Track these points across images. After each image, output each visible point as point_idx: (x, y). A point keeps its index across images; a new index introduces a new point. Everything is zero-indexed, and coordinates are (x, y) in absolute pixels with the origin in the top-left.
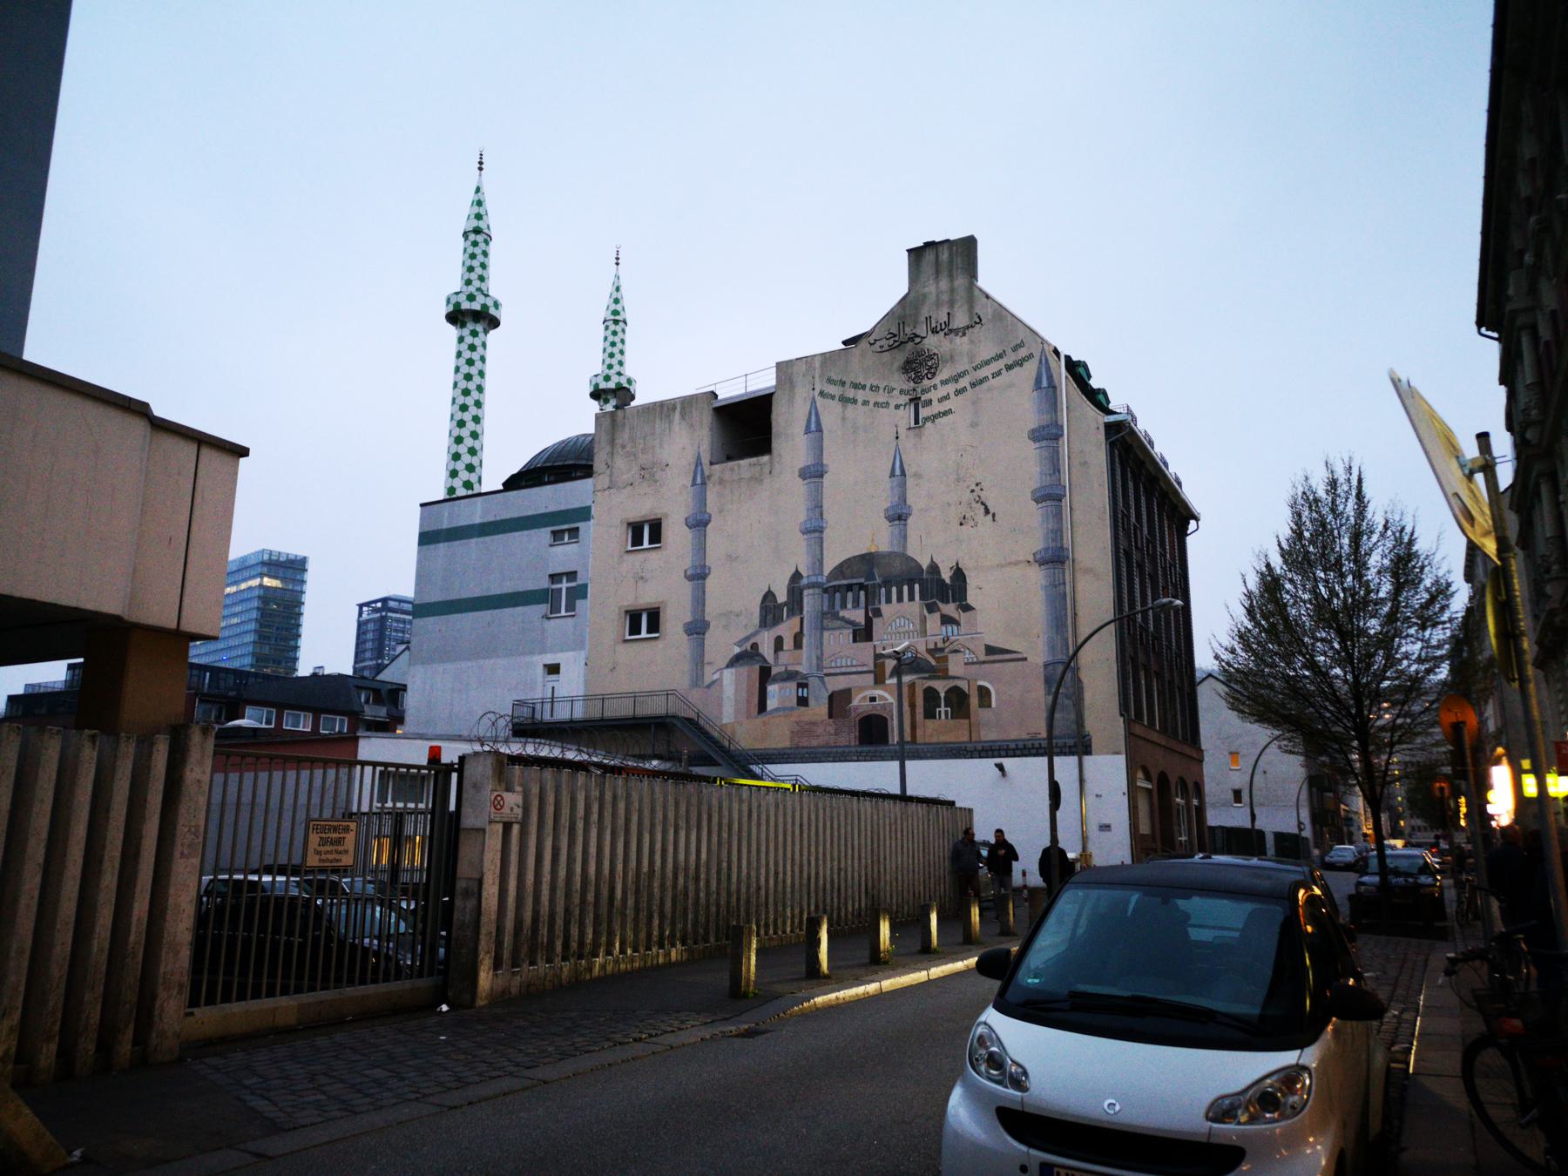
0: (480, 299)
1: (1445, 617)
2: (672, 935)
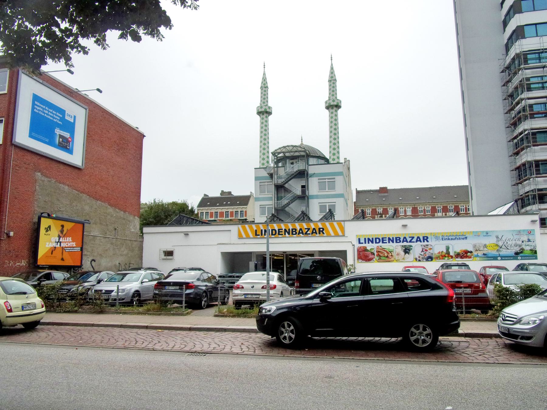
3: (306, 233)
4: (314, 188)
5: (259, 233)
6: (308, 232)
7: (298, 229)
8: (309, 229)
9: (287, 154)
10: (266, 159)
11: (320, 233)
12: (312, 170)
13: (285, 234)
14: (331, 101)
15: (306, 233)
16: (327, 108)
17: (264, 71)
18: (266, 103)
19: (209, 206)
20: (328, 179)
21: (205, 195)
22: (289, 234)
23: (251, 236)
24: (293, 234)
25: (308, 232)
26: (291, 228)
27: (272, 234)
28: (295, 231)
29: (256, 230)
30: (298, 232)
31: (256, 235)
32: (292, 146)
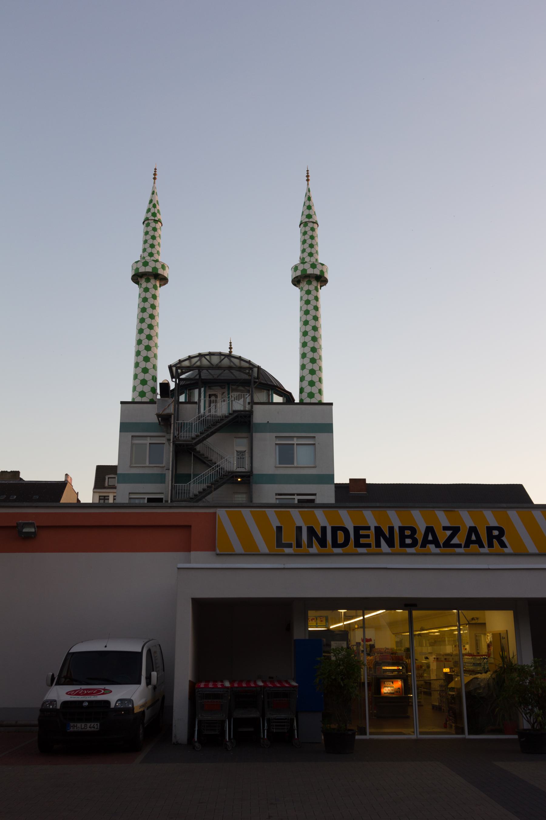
0: (152, 264)
1: (422, 683)
2: (187, 430)
3: (447, 544)
5: (289, 537)
6: (455, 541)
7: (421, 528)
8: (455, 530)
9: (205, 375)
11: (491, 545)
12: (261, 415)
13: (378, 545)
14: (307, 266)
15: (447, 544)
16: (296, 282)
20: (298, 437)
22: (391, 544)
23: (263, 548)
24: (403, 545)
25: (455, 541)
26: (397, 524)
27: (335, 544)
28: (411, 537)
29: (279, 529)
30: (419, 536)
31: (280, 544)
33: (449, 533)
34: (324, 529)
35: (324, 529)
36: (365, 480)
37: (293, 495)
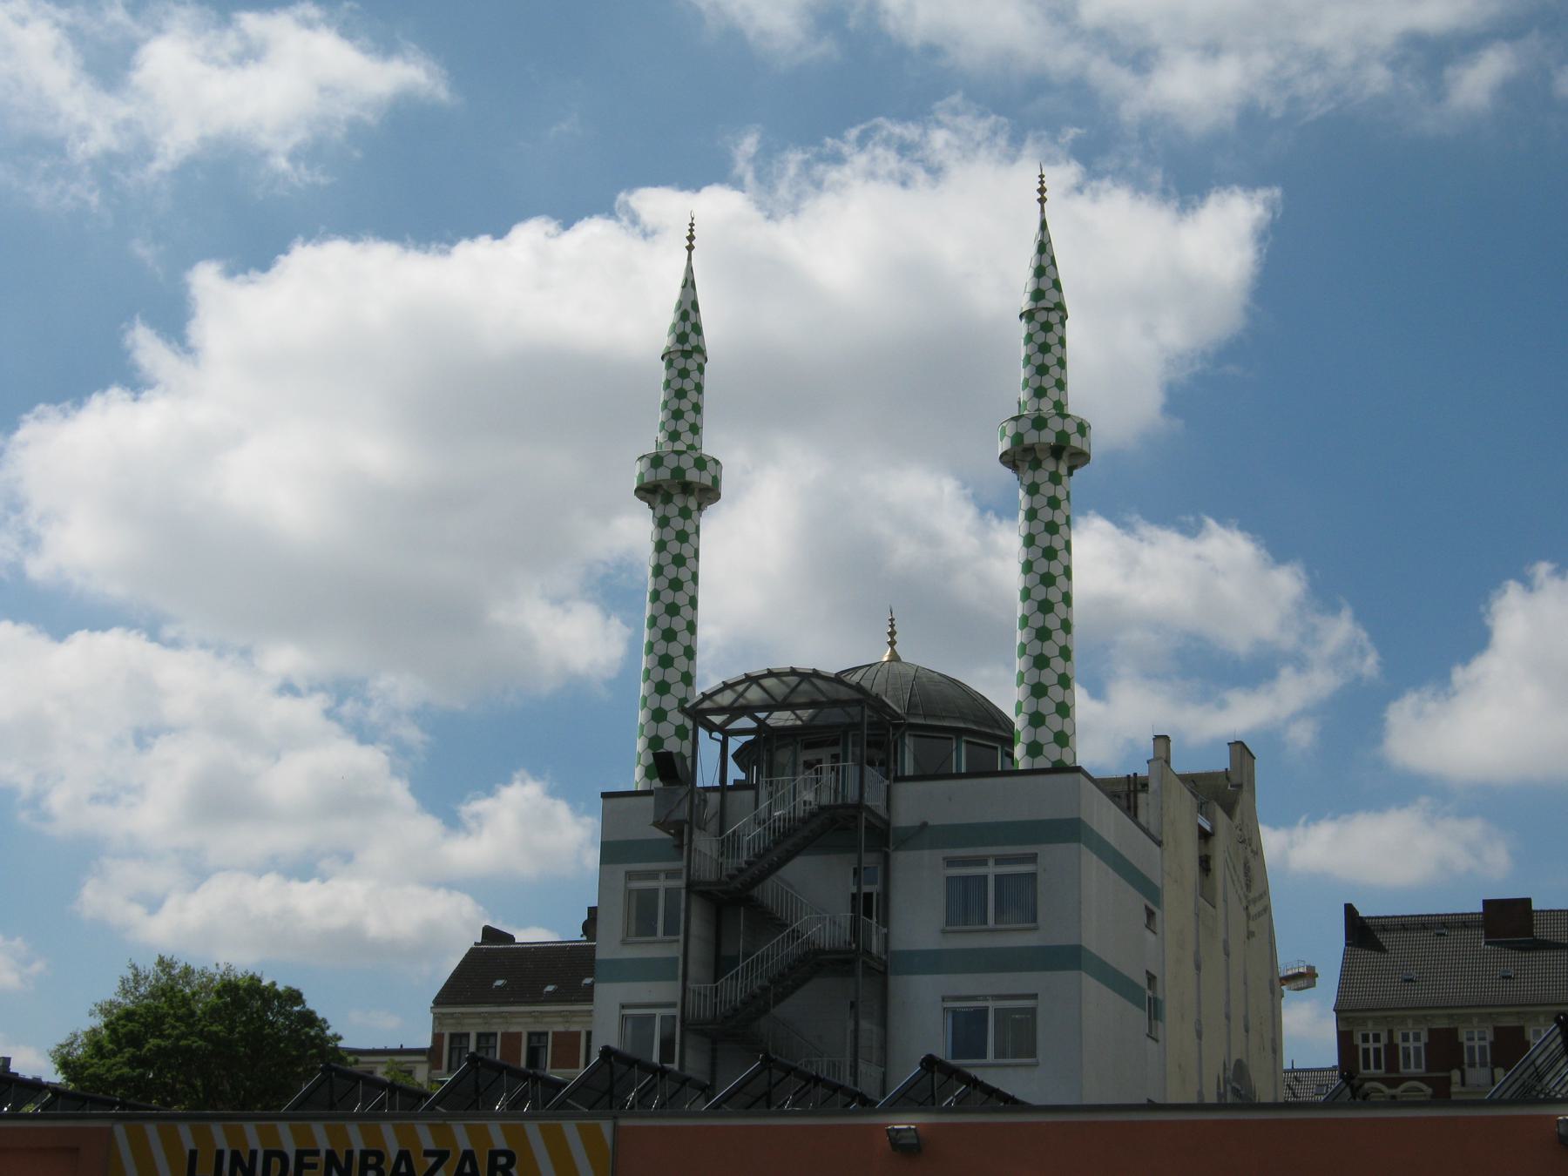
4: (918, 917)
7: (392, 1149)
8: (442, 1156)
9: (781, 719)
10: (1045, 735)
17: (690, 270)
18: (687, 438)
19: (501, 998)
20: (1000, 861)
21: (490, 934)
29: (193, 1153)
32: (793, 672)
33: (431, 1161)
34: (253, 1153)
35: (253, 1153)
36: (1527, 902)
37: (985, 998)
